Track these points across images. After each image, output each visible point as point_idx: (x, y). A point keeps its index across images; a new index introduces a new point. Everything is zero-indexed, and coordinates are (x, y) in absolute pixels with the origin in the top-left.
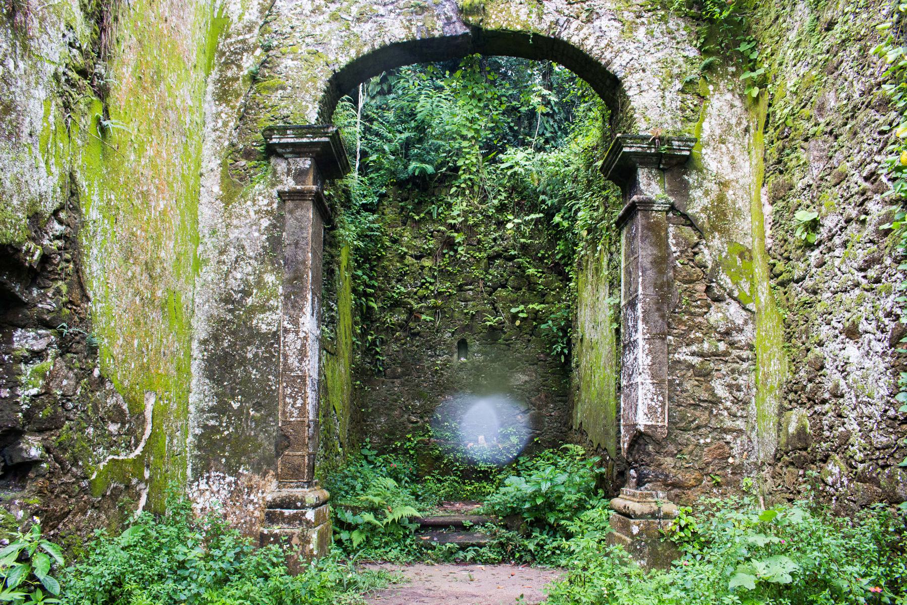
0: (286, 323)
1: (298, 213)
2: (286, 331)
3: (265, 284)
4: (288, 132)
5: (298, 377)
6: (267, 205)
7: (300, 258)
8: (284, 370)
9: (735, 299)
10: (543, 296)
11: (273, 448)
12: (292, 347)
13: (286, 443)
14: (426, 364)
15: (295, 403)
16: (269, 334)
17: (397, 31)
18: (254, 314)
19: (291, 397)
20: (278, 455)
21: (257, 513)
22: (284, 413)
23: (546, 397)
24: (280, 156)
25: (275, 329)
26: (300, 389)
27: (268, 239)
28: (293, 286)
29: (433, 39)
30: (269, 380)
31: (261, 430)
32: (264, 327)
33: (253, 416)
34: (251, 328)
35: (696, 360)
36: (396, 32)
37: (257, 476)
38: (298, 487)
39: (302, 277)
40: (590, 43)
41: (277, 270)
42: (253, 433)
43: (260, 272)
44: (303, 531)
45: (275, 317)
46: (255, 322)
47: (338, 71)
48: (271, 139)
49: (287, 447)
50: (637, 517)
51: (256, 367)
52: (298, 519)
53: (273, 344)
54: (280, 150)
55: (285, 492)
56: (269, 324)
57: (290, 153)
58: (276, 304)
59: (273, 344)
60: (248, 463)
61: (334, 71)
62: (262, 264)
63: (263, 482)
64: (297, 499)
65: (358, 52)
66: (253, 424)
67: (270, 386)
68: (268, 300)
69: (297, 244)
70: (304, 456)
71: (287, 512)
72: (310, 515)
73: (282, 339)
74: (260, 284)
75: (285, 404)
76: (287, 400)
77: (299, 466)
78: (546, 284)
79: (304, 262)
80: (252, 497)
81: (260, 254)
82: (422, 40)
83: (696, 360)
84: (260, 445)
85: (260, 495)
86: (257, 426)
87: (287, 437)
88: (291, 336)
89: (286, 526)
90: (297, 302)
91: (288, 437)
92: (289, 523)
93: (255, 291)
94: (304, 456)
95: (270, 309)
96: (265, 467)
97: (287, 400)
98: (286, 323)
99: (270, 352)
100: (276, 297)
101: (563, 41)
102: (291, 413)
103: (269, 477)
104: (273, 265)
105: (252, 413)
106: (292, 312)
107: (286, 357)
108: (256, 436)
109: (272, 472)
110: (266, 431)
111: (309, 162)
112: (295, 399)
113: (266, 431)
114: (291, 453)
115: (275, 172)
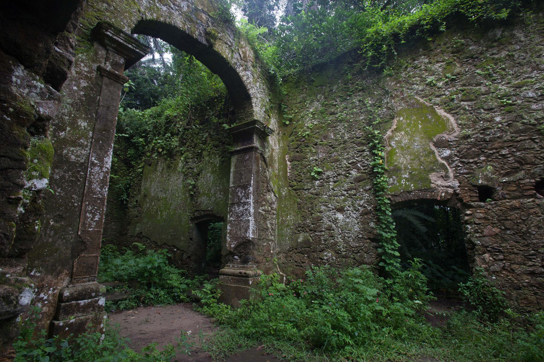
0: (93, 158)
1: (111, 88)
2: (93, 164)
3: (78, 126)
4: (121, 34)
5: (99, 198)
6: (88, 72)
7: (110, 118)
8: (88, 192)
9: (273, 192)
10: (116, 172)
11: (69, 252)
12: (96, 177)
13: (83, 248)
14: (31, 195)
15: (94, 217)
16: (77, 163)
17: (178, 21)
18: (65, 146)
19: (91, 212)
20: (73, 257)
21: (45, 309)
22: (84, 224)
23: (111, 219)
24: (104, 46)
25: (82, 161)
26: (99, 208)
27: (85, 95)
28: (102, 135)
29: (193, 37)
30: (72, 198)
31: (60, 238)
32: (73, 157)
33: (53, 226)
34: (61, 155)
35: (264, 213)
36: (178, 22)
37: (50, 277)
38: (89, 281)
39: (109, 131)
40: (245, 78)
41: (89, 119)
42: (50, 240)
43: (75, 116)
44: (96, 315)
45: (84, 152)
46: (65, 151)
47: (144, 19)
48: (107, 31)
49: (82, 251)
50: (251, 277)
51: (61, 187)
52: (93, 306)
53: (80, 171)
54: (107, 41)
55: (79, 287)
56: (77, 156)
57: (113, 48)
58: (86, 143)
59: (80, 171)
60: (42, 266)
61: (142, 18)
62: (77, 111)
63: (56, 281)
64: (92, 291)
65: (158, 18)
66: (52, 233)
67: (73, 203)
68: (79, 138)
69: (108, 108)
70: (97, 257)
71: (82, 303)
72: (102, 301)
73: (89, 169)
74: (73, 124)
75: (86, 218)
76: (88, 215)
77: (93, 265)
78: (118, 167)
79: (112, 122)
80: (42, 295)
81: (77, 104)
82: (188, 34)
83: (264, 213)
84: (57, 250)
85: (50, 292)
86: (56, 233)
87: (83, 243)
88: (97, 169)
89: (80, 314)
90: (104, 146)
91: (85, 243)
92: (83, 312)
93: (68, 129)
94: (97, 257)
95: (80, 146)
96: (59, 268)
97: (88, 215)
98: (93, 158)
99: (76, 177)
100: (87, 138)
101: (236, 72)
102: (90, 224)
103: (62, 276)
104: (87, 115)
105: (52, 223)
106: (99, 152)
107: (91, 183)
108: (54, 242)
109: (66, 271)
110: (64, 238)
111: (123, 61)
112: (94, 215)
113: (64, 238)
114: (86, 255)
115: (96, 54)
